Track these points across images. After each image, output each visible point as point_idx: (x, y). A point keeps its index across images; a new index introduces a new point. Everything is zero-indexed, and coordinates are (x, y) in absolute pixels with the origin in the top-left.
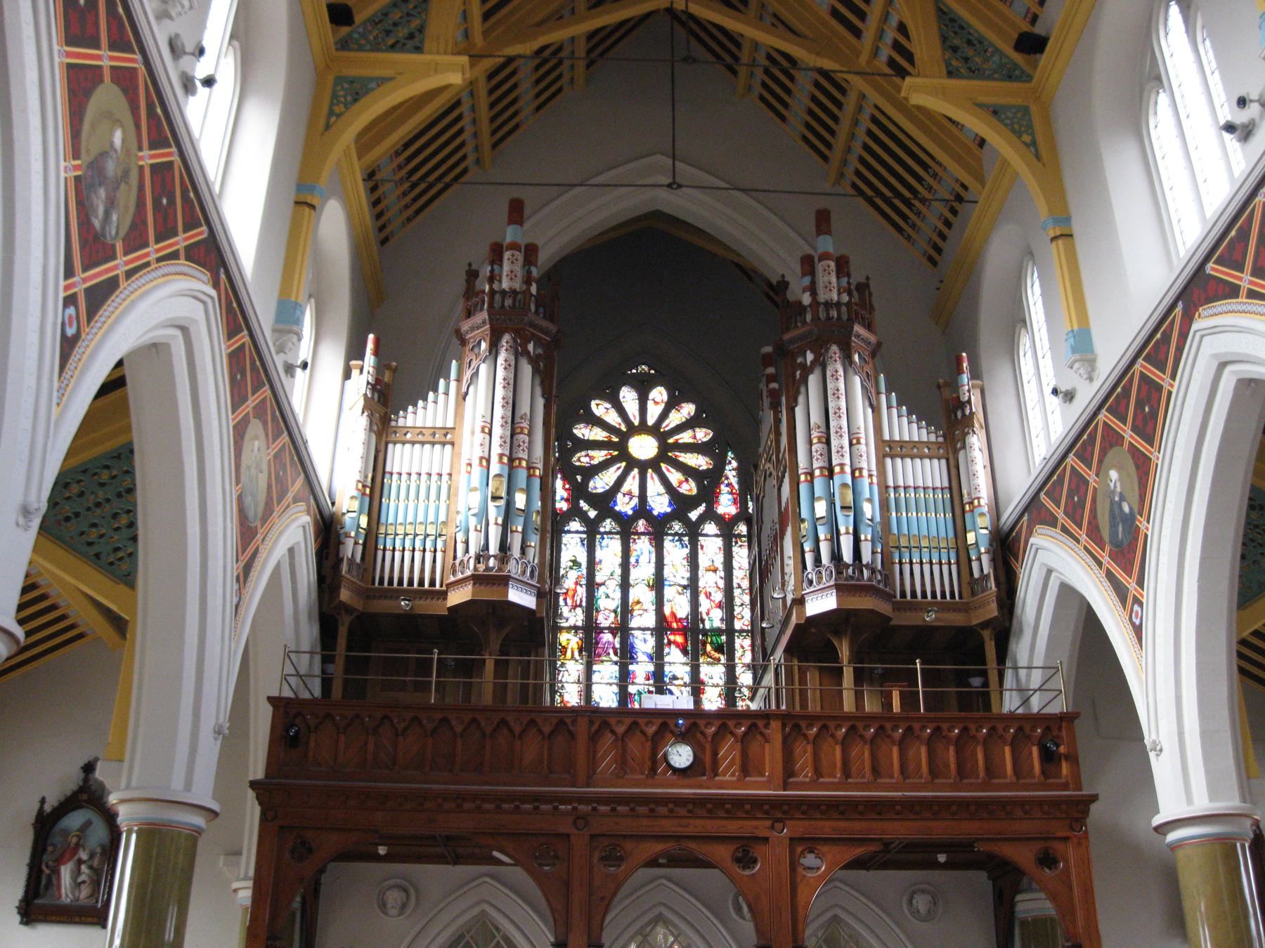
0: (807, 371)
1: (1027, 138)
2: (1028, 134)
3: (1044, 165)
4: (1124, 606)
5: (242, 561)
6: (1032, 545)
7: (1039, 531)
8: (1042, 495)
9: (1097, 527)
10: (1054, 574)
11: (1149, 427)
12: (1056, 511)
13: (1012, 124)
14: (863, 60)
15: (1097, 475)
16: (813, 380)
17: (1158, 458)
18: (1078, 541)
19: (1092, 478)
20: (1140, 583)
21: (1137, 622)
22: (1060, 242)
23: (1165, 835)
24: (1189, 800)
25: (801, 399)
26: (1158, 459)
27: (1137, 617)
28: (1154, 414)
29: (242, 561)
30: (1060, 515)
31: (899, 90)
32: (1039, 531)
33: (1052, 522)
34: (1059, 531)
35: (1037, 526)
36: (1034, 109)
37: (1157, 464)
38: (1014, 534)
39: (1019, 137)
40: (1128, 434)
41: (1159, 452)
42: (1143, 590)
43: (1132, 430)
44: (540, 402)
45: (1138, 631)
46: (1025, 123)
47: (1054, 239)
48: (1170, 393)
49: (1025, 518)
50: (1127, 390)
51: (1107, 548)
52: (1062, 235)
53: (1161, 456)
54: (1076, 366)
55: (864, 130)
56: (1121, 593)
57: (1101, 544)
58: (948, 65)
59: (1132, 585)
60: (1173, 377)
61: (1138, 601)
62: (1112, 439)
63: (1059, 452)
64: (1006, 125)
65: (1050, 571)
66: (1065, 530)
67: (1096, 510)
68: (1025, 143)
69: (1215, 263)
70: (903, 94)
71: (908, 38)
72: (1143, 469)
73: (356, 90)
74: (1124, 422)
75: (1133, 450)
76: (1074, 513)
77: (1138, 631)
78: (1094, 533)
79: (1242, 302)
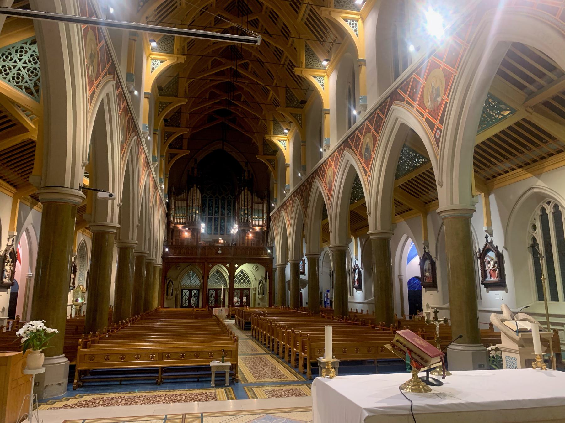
0: (242, 191)
5: (96, 84)
9: (362, 153)
11: (378, 128)
12: (405, 96)
15: (363, 139)
16: (243, 192)
21: (438, 137)
22: (303, 146)
23: (440, 214)
25: (241, 195)
28: (380, 126)
29: (96, 84)
30: (352, 146)
31: (293, 69)
38: (422, 66)
40: (373, 130)
41: (457, 70)
42: (442, 125)
44: (200, 195)
45: (437, 141)
47: (302, 145)
49: (389, 99)
50: (374, 117)
51: (364, 159)
54: (361, 107)
55: (306, 18)
58: (287, 103)
59: (368, 171)
62: (368, 130)
65: (397, 119)
66: (408, 103)
67: (423, 95)
69: (416, 73)
70: (294, 71)
72: (375, 139)
73: (167, 104)
75: (373, 135)
78: (361, 154)
79: (404, 104)
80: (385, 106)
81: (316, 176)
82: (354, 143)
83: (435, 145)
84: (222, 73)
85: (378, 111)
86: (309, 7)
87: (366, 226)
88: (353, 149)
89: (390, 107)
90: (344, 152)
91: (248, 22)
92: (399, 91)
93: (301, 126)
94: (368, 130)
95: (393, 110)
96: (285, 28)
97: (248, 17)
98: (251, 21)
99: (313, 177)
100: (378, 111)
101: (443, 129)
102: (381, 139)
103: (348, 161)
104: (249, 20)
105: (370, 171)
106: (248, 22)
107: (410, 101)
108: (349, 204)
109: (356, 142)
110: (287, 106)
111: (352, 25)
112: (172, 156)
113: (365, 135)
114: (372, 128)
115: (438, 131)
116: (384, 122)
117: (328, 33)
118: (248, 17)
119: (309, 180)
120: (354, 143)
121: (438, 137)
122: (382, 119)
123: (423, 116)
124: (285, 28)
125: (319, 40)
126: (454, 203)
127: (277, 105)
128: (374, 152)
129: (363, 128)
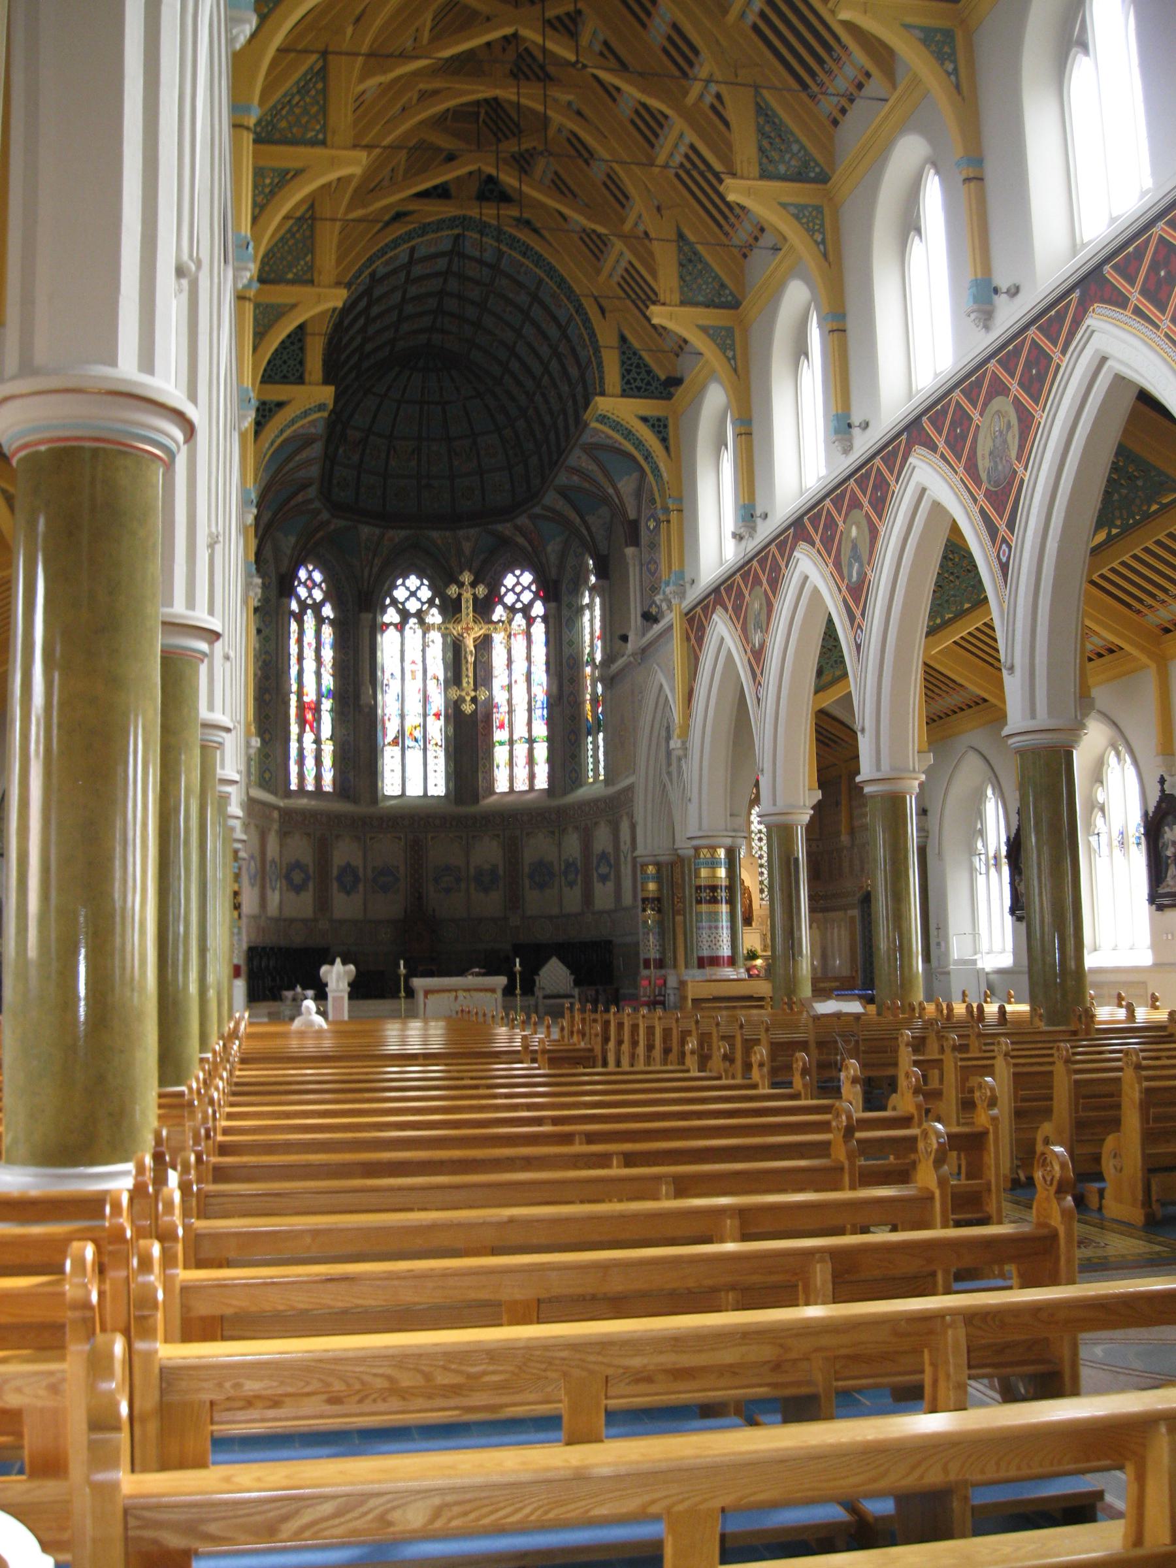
1: (819, 237)
2: (820, 233)
3: (963, 99)
4: (994, 543)
6: (1089, 326)
7: (918, 451)
8: (924, 419)
10: (1109, 363)
13: (807, 223)
14: (627, 227)
15: (981, 415)
17: (1041, 417)
18: (956, 473)
19: (975, 415)
20: (1011, 526)
21: (1004, 560)
24: (1033, 716)
26: (1041, 417)
27: (1004, 551)
30: (941, 444)
31: (647, 307)
32: (918, 451)
33: (1120, 301)
34: (1129, 314)
35: (1096, 305)
36: (827, 211)
37: (1040, 423)
39: (812, 236)
40: (1014, 387)
41: (1043, 411)
43: (1139, 293)
45: (1004, 567)
46: (818, 222)
48: (1058, 367)
49: (904, 437)
52: (974, 178)
53: (1045, 415)
56: (851, 617)
57: (978, 482)
60: (1064, 352)
61: (859, 627)
62: (855, 504)
63: (774, 533)
64: (802, 224)
65: (1104, 360)
68: (816, 242)
69: (1167, 223)
71: (724, 107)
72: (1026, 422)
74: (1013, 377)
75: (1017, 403)
76: (956, 444)
77: (1004, 567)
79: (1126, 315)
80: (1061, 316)
81: (718, 607)
82: (869, 492)
83: (1000, 580)
84: (466, 65)
85: (877, 461)
86: (713, 88)
87: (852, 759)
88: (942, 454)
89: (1077, 323)
90: (911, 460)
91: (549, 23)
92: (1108, 272)
93: (735, 370)
94: (855, 504)
95: (1093, 332)
96: (596, 251)
97: (543, 7)
98: (558, 18)
99: (707, 606)
100: (957, 395)
101: (1013, 545)
102: (888, 531)
103: (924, 490)
104: (551, 14)
105: (863, 614)
106: (549, 23)
107: (1150, 309)
108: (812, 695)
109: (875, 488)
110: (683, 303)
111: (661, 424)
112: (265, 412)
113: (985, 405)
114: (865, 503)
115: (1004, 546)
116: (894, 492)
117: (837, 60)
118: (543, 7)
119: (750, 570)
120: (869, 492)
121: (1004, 560)
122: (1050, 359)
123: (975, 500)
124: (596, 251)
125: (805, 86)
126: (883, 768)
127: (649, 298)
128: (871, 565)
129: (945, 410)
